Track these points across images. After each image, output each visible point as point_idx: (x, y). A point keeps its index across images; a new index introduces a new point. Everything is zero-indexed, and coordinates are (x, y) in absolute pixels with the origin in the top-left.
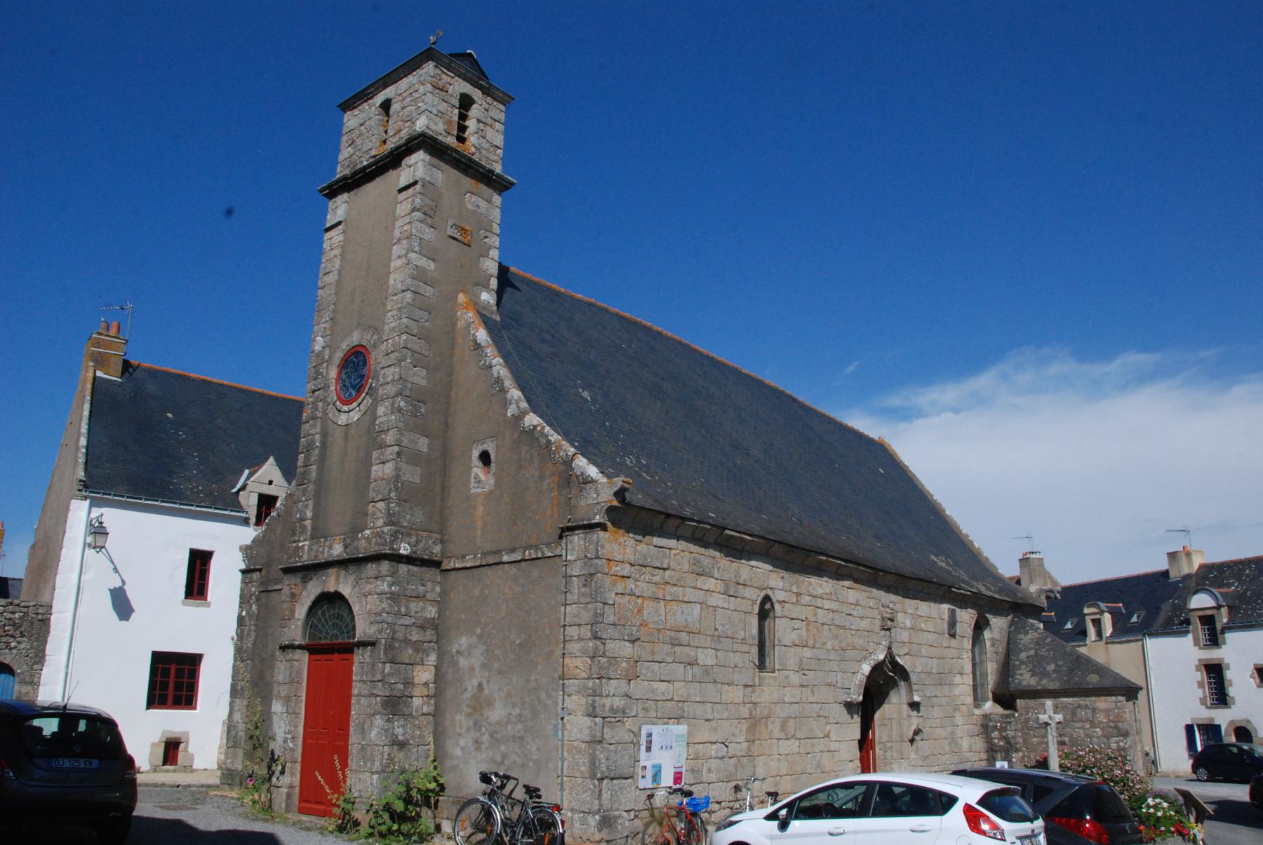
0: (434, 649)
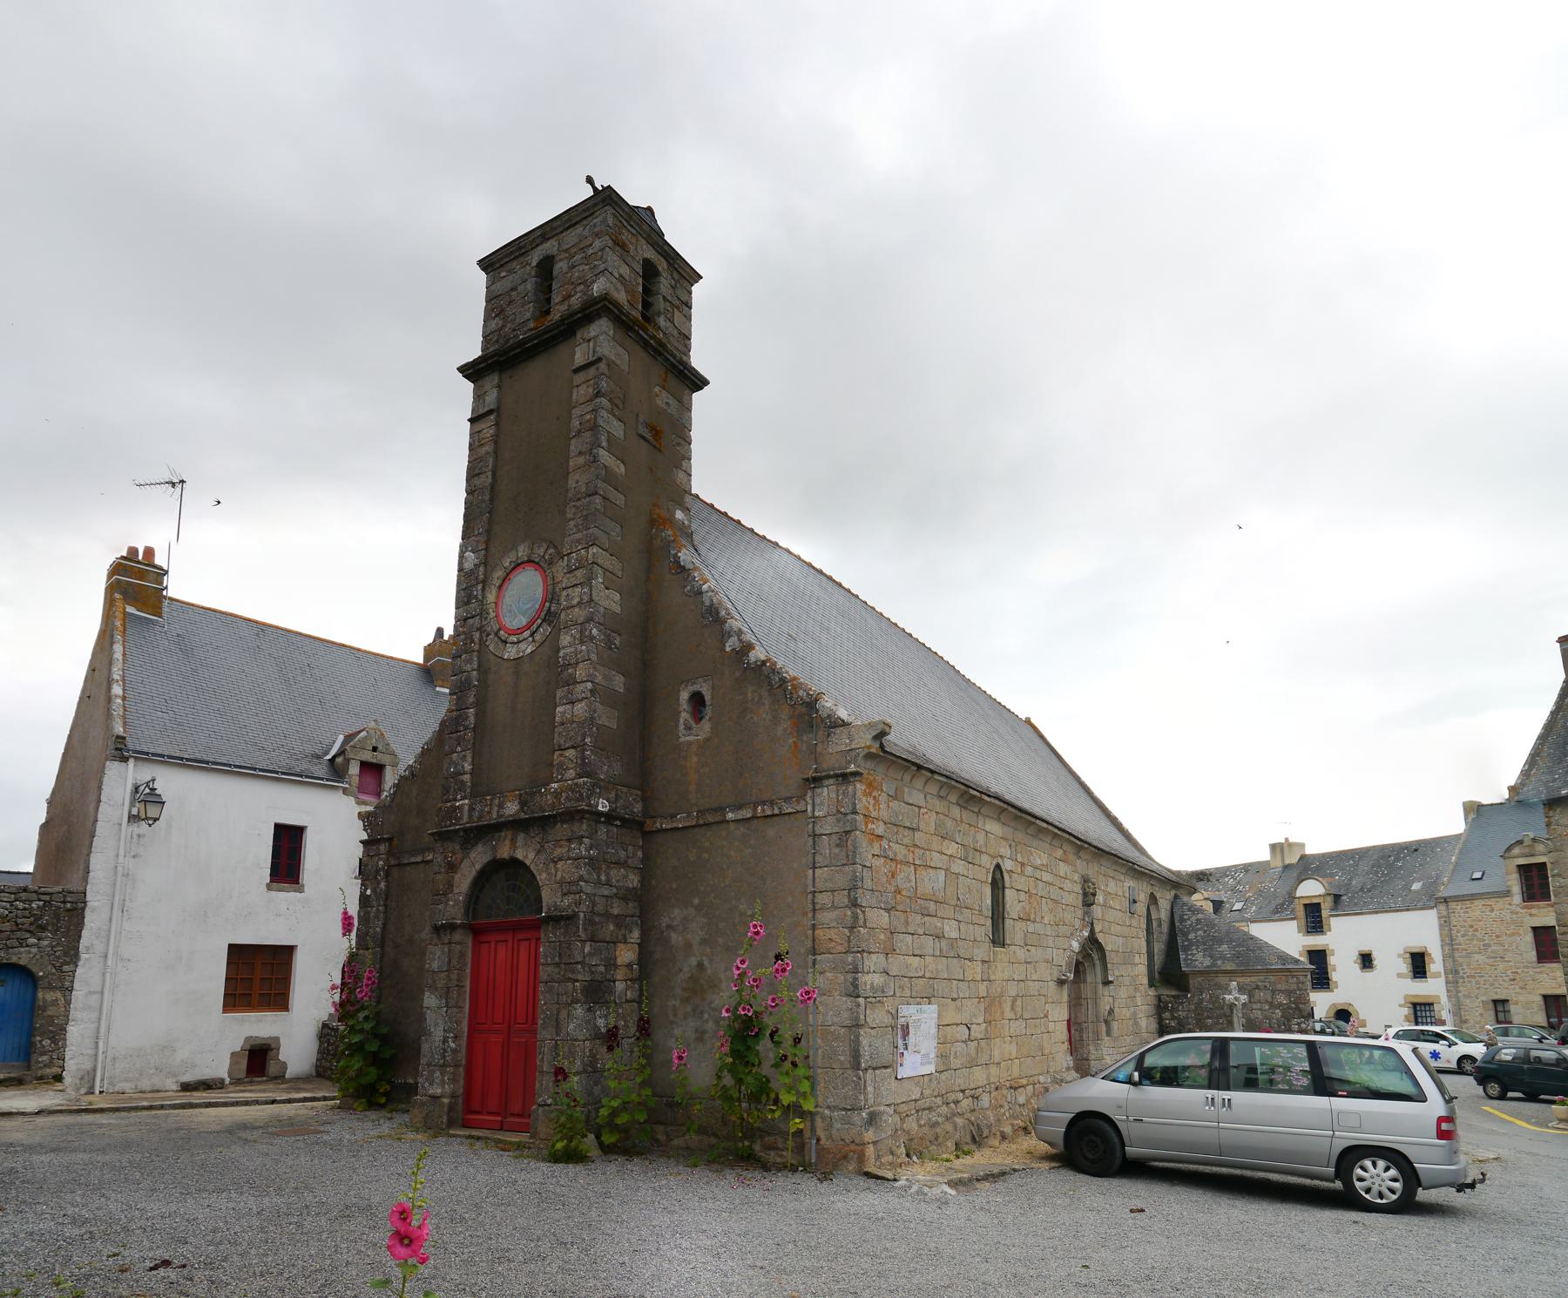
0: (637, 924)
